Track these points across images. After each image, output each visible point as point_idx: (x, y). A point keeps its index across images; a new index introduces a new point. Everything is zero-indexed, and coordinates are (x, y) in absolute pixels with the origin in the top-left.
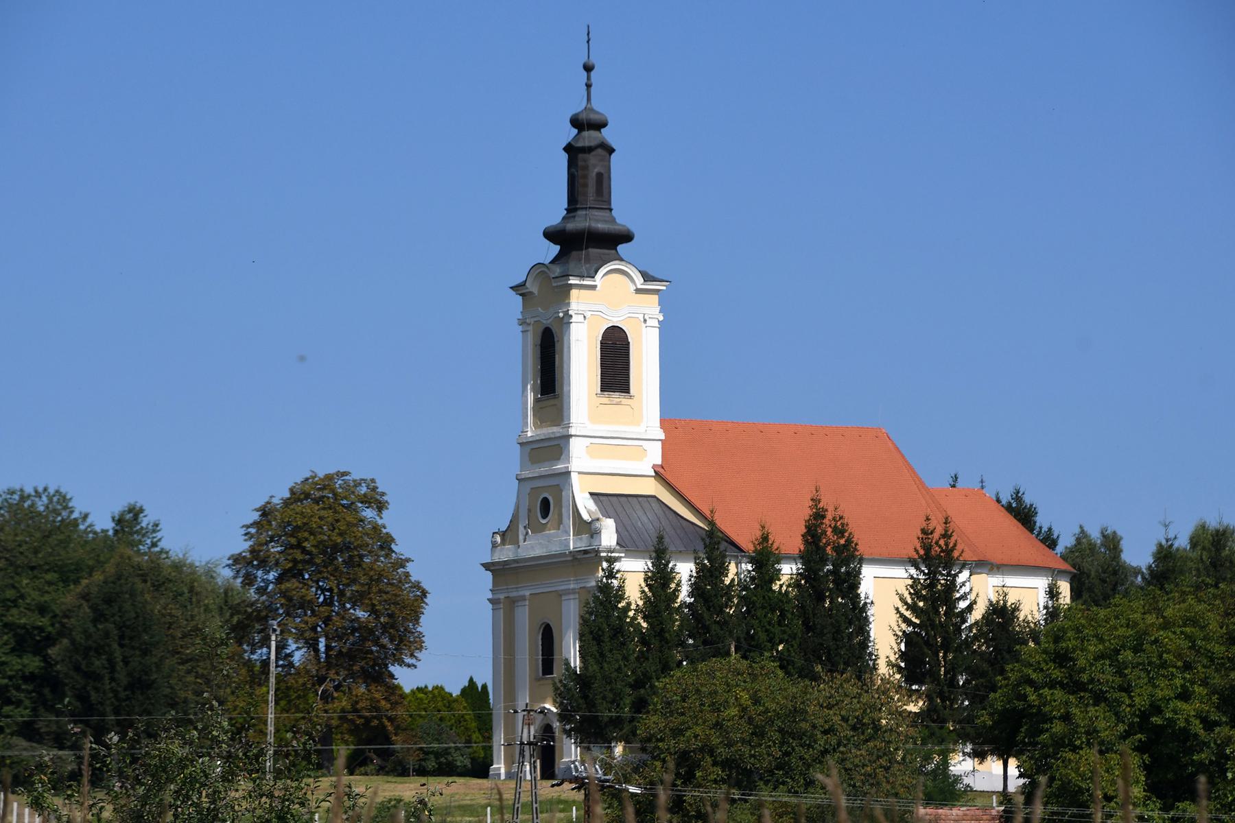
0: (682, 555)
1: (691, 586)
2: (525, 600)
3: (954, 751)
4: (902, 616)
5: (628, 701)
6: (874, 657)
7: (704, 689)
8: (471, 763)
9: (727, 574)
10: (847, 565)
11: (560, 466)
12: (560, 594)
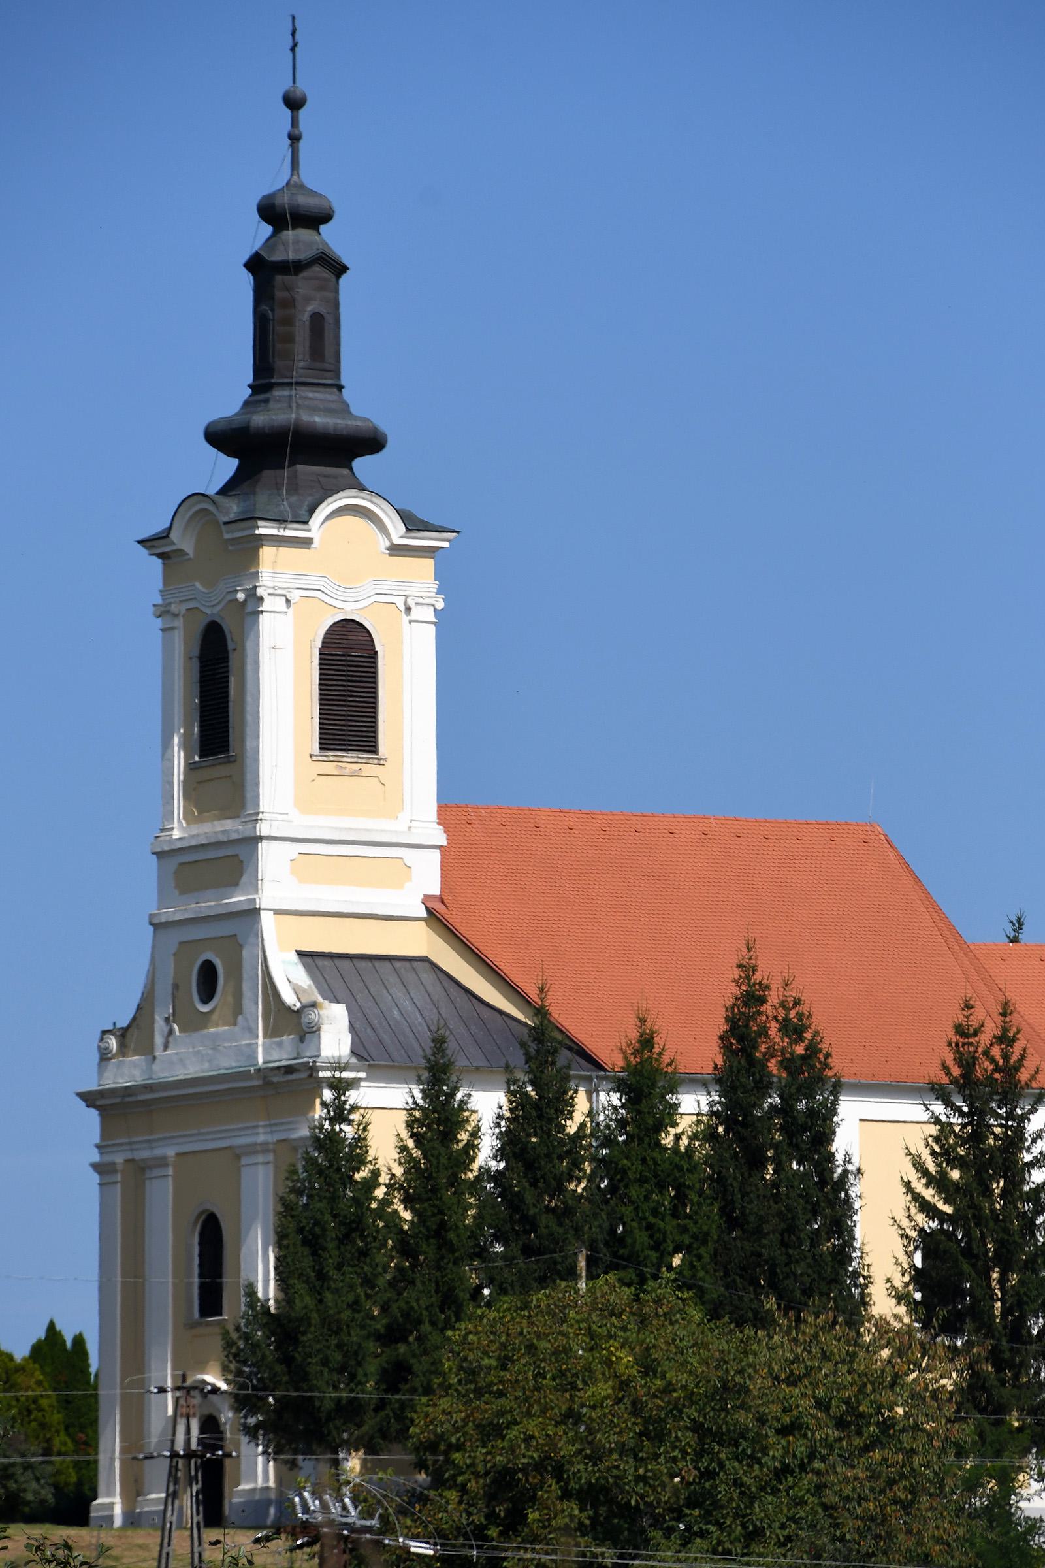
0: (482, 1076)
1: (501, 1136)
2: (166, 1165)
3: (1021, 1469)
4: (917, 1197)
5: (372, 1366)
6: (862, 1280)
7: (544, 1344)
8: (54, 1495)
9: (571, 1113)
10: (810, 1097)
11: (237, 899)
12: (236, 1155)
